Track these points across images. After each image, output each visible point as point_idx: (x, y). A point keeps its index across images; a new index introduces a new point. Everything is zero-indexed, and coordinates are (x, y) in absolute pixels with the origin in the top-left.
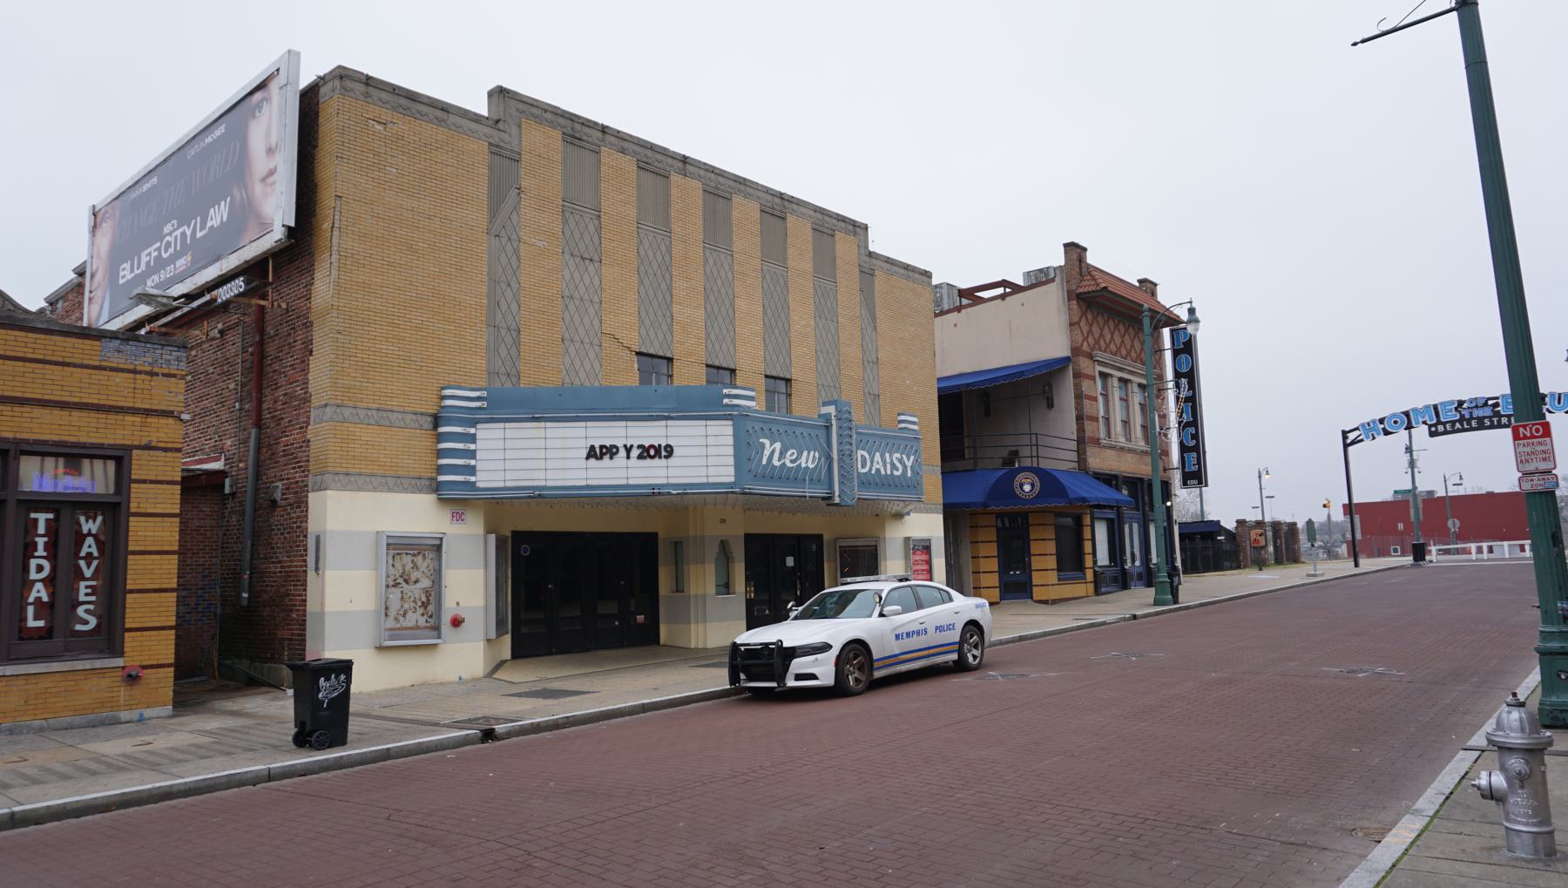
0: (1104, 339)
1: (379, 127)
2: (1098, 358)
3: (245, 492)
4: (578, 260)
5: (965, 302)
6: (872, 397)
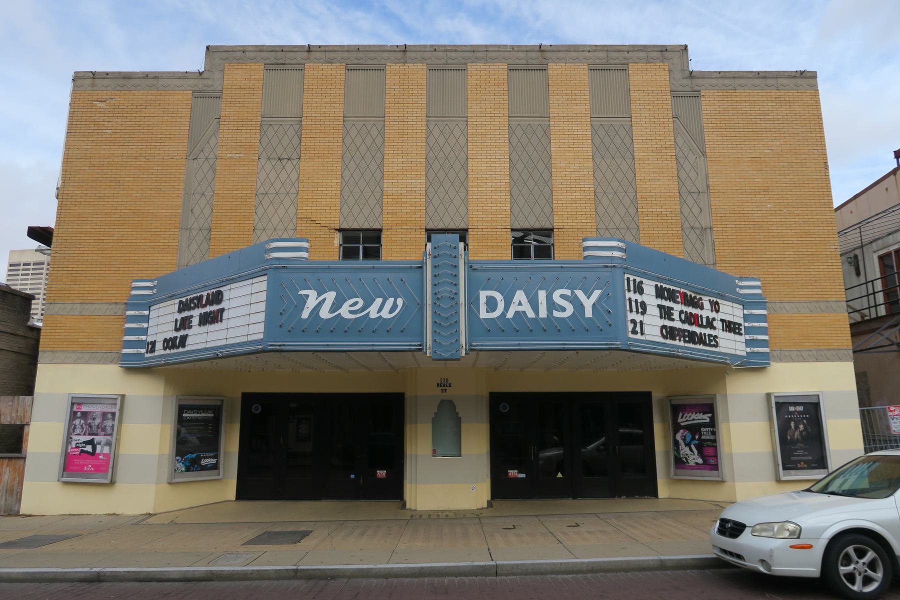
1: (103, 105)
6: (698, 232)
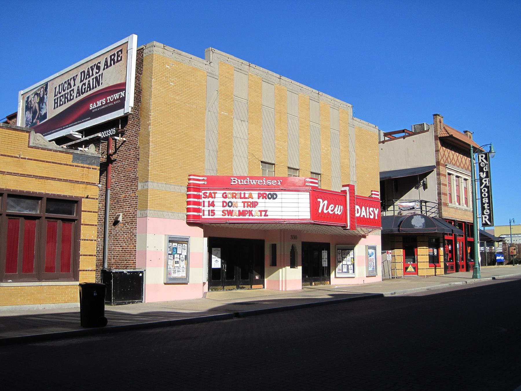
0: (450, 158)
2: (447, 167)
3: (110, 216)
4: (239, 121)
5: (387, 139)
